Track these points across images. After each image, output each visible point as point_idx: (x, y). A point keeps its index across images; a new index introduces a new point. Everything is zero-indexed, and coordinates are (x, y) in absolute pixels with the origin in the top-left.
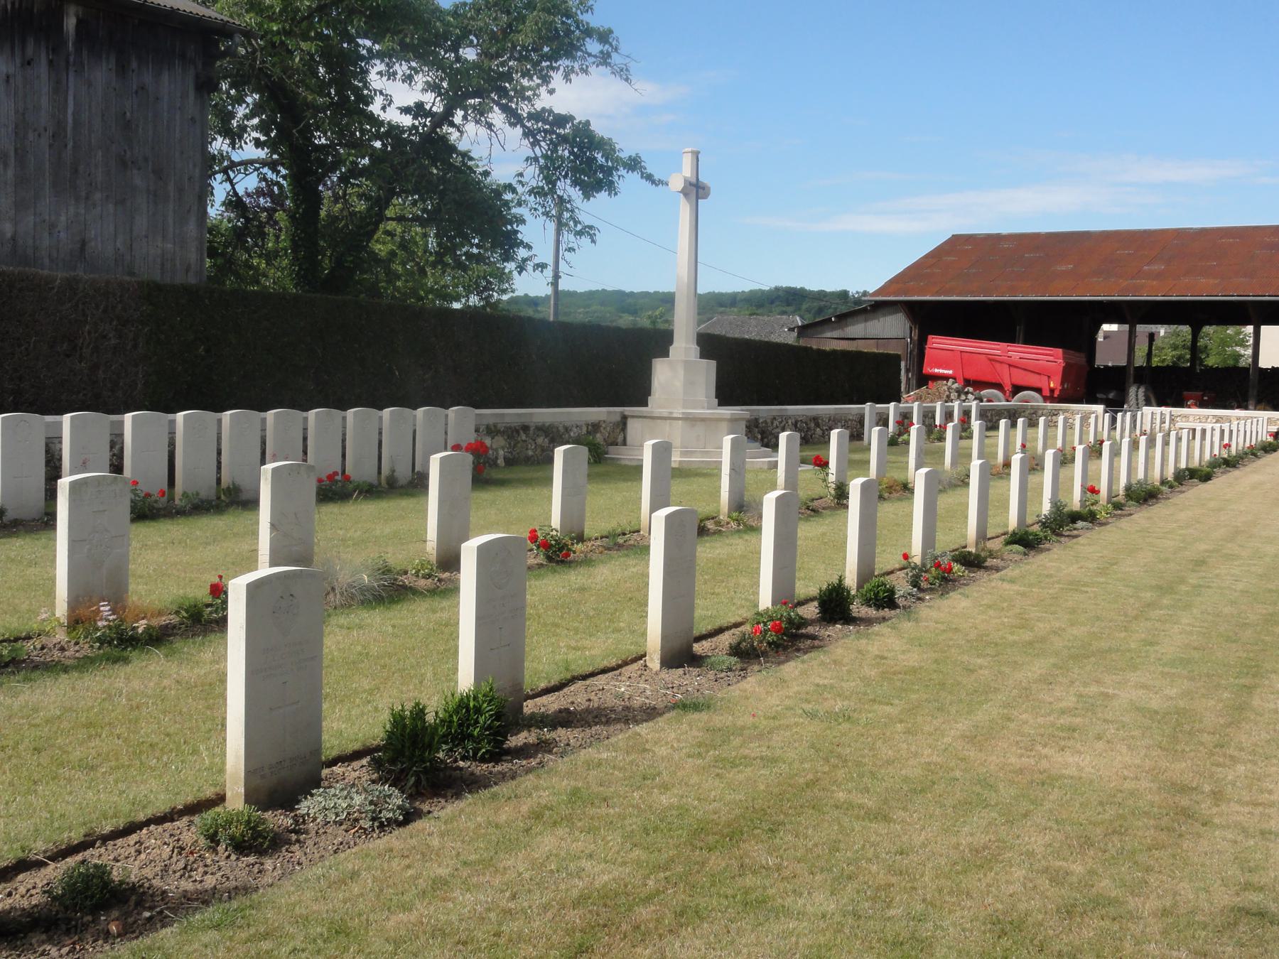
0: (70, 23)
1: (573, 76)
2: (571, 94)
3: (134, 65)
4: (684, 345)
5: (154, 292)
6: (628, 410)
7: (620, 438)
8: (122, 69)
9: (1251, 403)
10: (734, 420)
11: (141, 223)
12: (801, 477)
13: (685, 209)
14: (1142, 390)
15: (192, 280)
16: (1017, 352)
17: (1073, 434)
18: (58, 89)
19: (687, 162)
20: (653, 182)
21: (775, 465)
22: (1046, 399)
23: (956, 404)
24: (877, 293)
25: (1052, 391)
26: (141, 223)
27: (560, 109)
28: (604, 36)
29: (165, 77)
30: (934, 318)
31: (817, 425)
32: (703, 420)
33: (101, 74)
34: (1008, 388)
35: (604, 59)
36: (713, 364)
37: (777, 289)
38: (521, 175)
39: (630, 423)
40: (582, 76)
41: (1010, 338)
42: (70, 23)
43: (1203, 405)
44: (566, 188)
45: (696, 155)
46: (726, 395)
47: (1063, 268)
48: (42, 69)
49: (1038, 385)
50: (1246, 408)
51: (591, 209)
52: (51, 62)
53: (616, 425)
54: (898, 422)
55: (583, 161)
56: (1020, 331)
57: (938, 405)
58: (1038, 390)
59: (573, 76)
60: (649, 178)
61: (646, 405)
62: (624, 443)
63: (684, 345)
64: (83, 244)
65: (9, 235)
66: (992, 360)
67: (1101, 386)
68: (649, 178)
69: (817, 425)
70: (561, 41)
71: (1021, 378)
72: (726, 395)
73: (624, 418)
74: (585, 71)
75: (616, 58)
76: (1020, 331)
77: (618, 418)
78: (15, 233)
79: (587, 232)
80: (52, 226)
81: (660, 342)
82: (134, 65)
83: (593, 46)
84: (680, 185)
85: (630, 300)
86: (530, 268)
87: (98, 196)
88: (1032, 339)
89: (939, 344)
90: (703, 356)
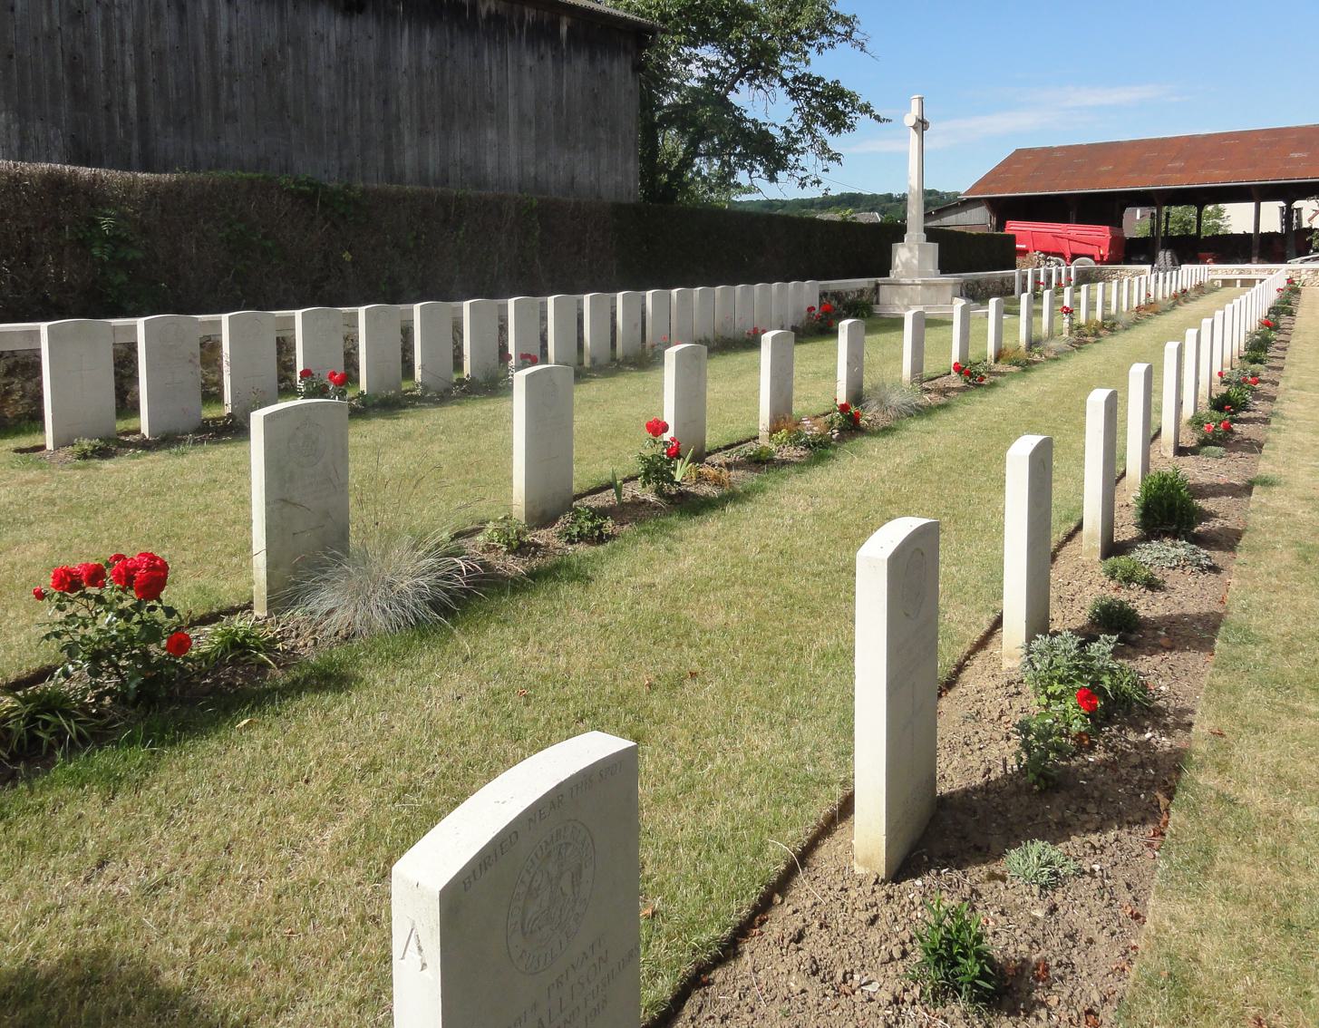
0: (564, 29)
1: (823, 50)
2: (828, 64)
3: (599, 56)
4: (915, 232)
5: (619, 209)
6: (880, 280)
7: (875, 300)
8: (592, 59)
9: (1255, 259)
10: (955, 284)
11: (604, 162)
12: (1004, 323)
13: (914, 136)
14: (1168, 254)
15: (632, 201)
16: (1073, 230)
17: (988, 281)
18: (558, 75)
19: (915, 105)
20: (879, 120)
21: (987, 315)
22: (1097, 262)
23: (1042, 270)
24: (966, 194)
25: (1102, 256)
26: (604, 162)
27: (815, 75)
28: (846, 21)
29: (615, 64)
30: (1006, 209)
31: (979, 286)
32: (935, 285)
33: (581, 63)
34: (1068, 256)
35: (848, 36)
36: (937, 244)
37: (842, 195)
38: (791, 120)
39: (882, 288)
40: (829, 50)
41: (1065, 220)
42: (564, 29)
43: (1216, 261)
44: (822, 131)
45: (921, 99)
46: (946, 266)
47: (1105, 168)
48: (549, 62)
49: (1091, 252)
50: (1249, 261)
51: (835, 142)
52: (553, 56)
53: (873, 290)
54: (1003, 279)
55: (832, 107)
56: (1072, 215)
57: (1030, 270)
58: (1092, 257)
59: (823, 50)
60: (877, 118)
61: (888, 276)
62: (878, 303)
63: (915, 232)
64: (573, 178)
65: (532, 174)
66: (1055, 236)
67: (1133, 251)
68: (877, 118)
69: (979, 286)
70: (828, 26)
71: (1077, 248)
72: (946, 266)
73: (877, 285)
74: (831, 45)
75: (855, 35)
76: (1072, 215)
77: (873, 286)
78: (536, 174)
79: (835, 157)
80: (556, 167)
81: (896, 232)
82: (599, 56)
83: (840, 29)
84: (913, 122)
85: (740, 207)
86: (808, 184)
87: (580, 146)
88: (1081, 220)
89: (1013, 227)
90: (928, 240)
